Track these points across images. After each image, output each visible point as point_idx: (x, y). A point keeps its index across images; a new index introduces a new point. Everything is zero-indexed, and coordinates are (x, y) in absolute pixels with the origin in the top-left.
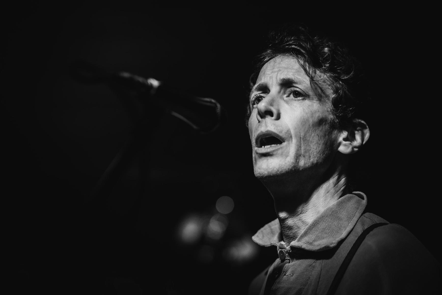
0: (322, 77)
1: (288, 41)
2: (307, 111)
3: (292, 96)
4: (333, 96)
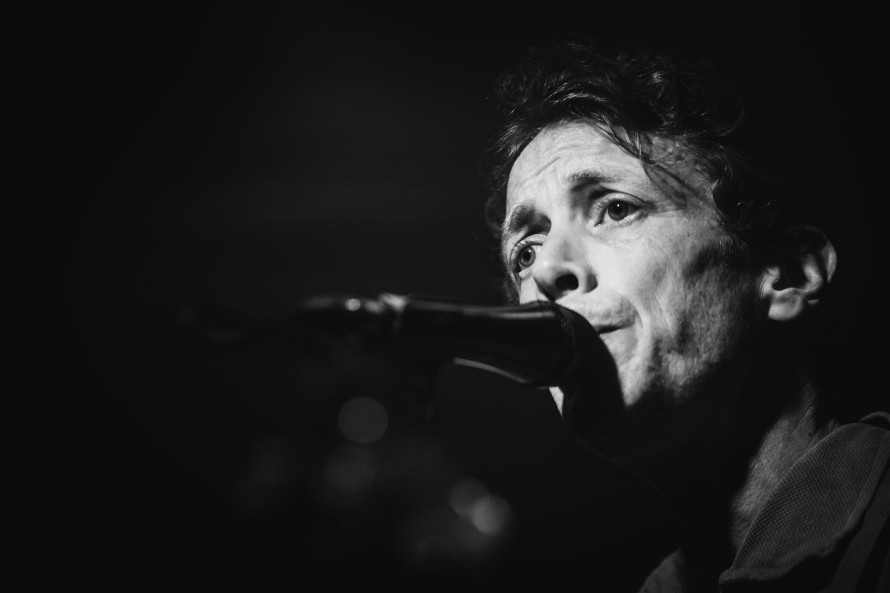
0: (665, 148)
2: (659, 243)
3: (607, 217)
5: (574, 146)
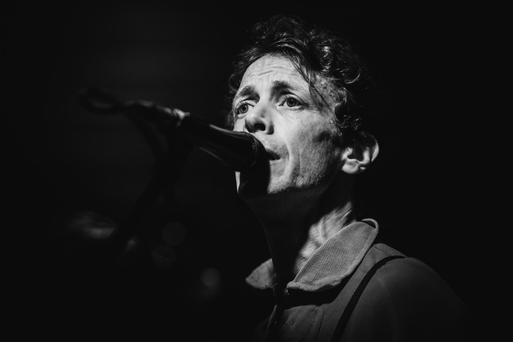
0: (322, 82)
1: (279, 39)
3: (286, 104)
4: (337, 104)
5: (280, 67)
